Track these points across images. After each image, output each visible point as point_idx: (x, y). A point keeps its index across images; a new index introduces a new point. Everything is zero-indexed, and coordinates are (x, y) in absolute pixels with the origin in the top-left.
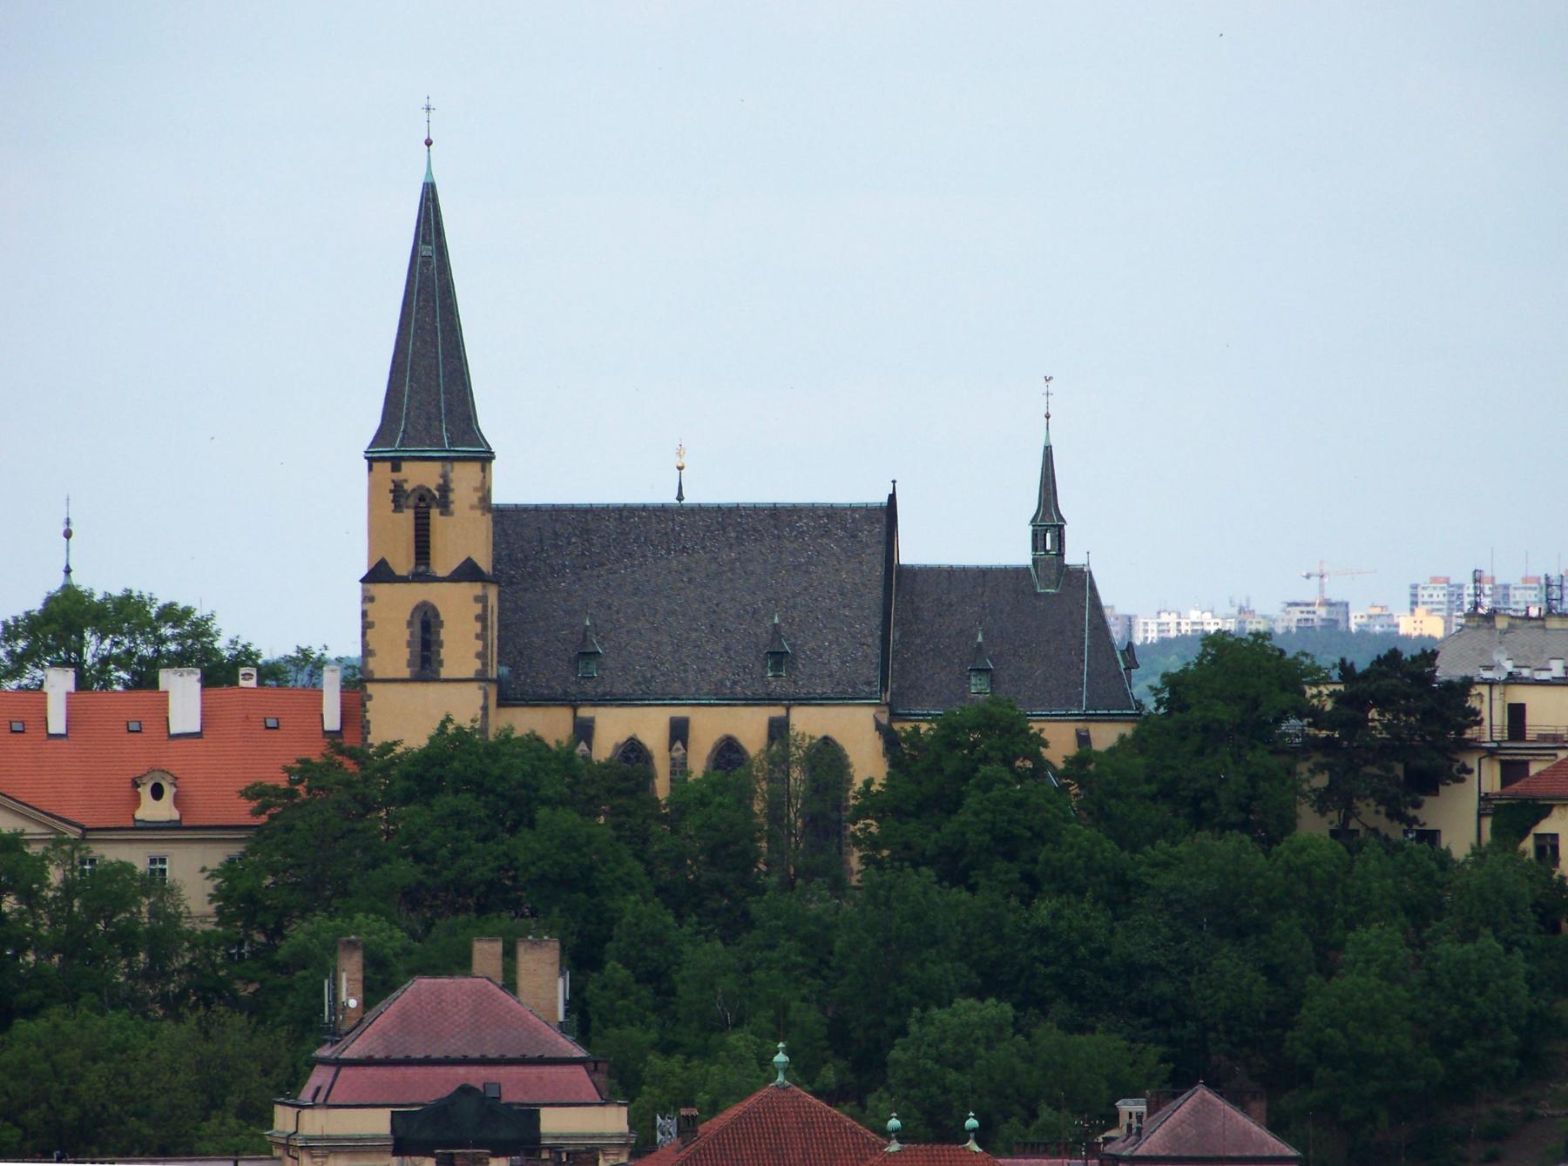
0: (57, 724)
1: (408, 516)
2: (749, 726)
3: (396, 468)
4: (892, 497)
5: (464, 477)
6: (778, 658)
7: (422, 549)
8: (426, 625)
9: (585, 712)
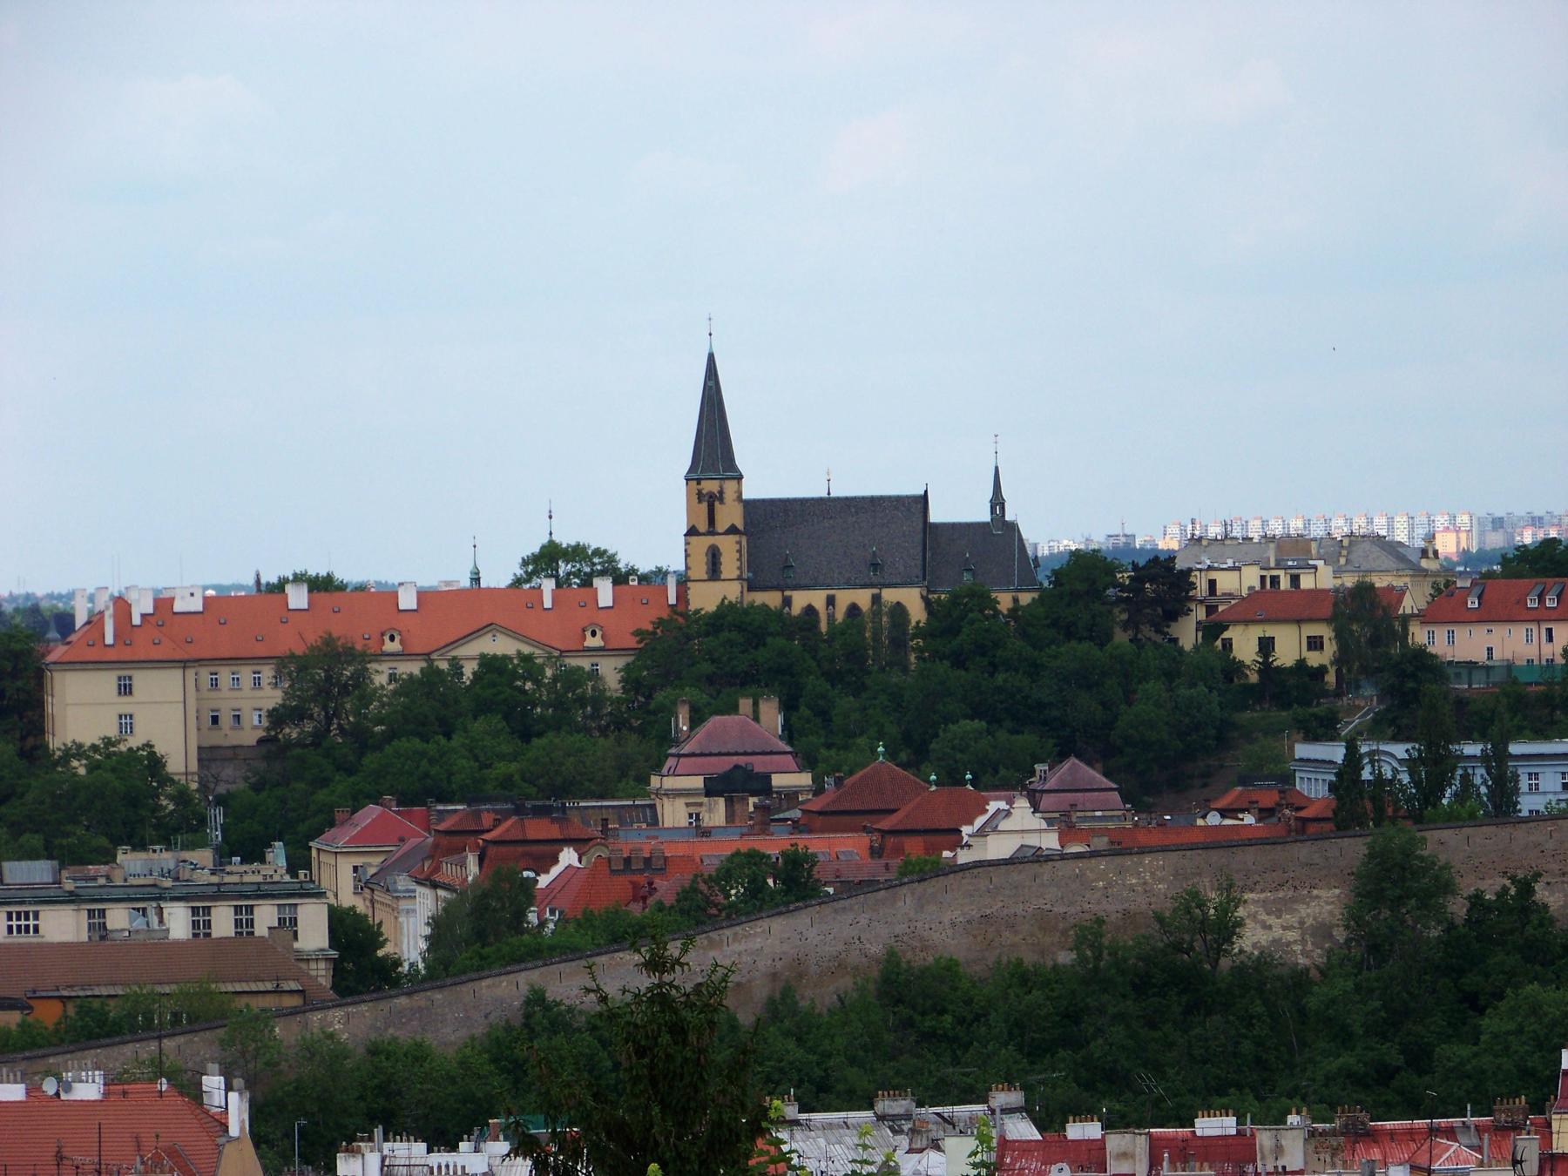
1: (705, 505)
5: (730, 487)
8: (714, 556)
9: (787, 593)
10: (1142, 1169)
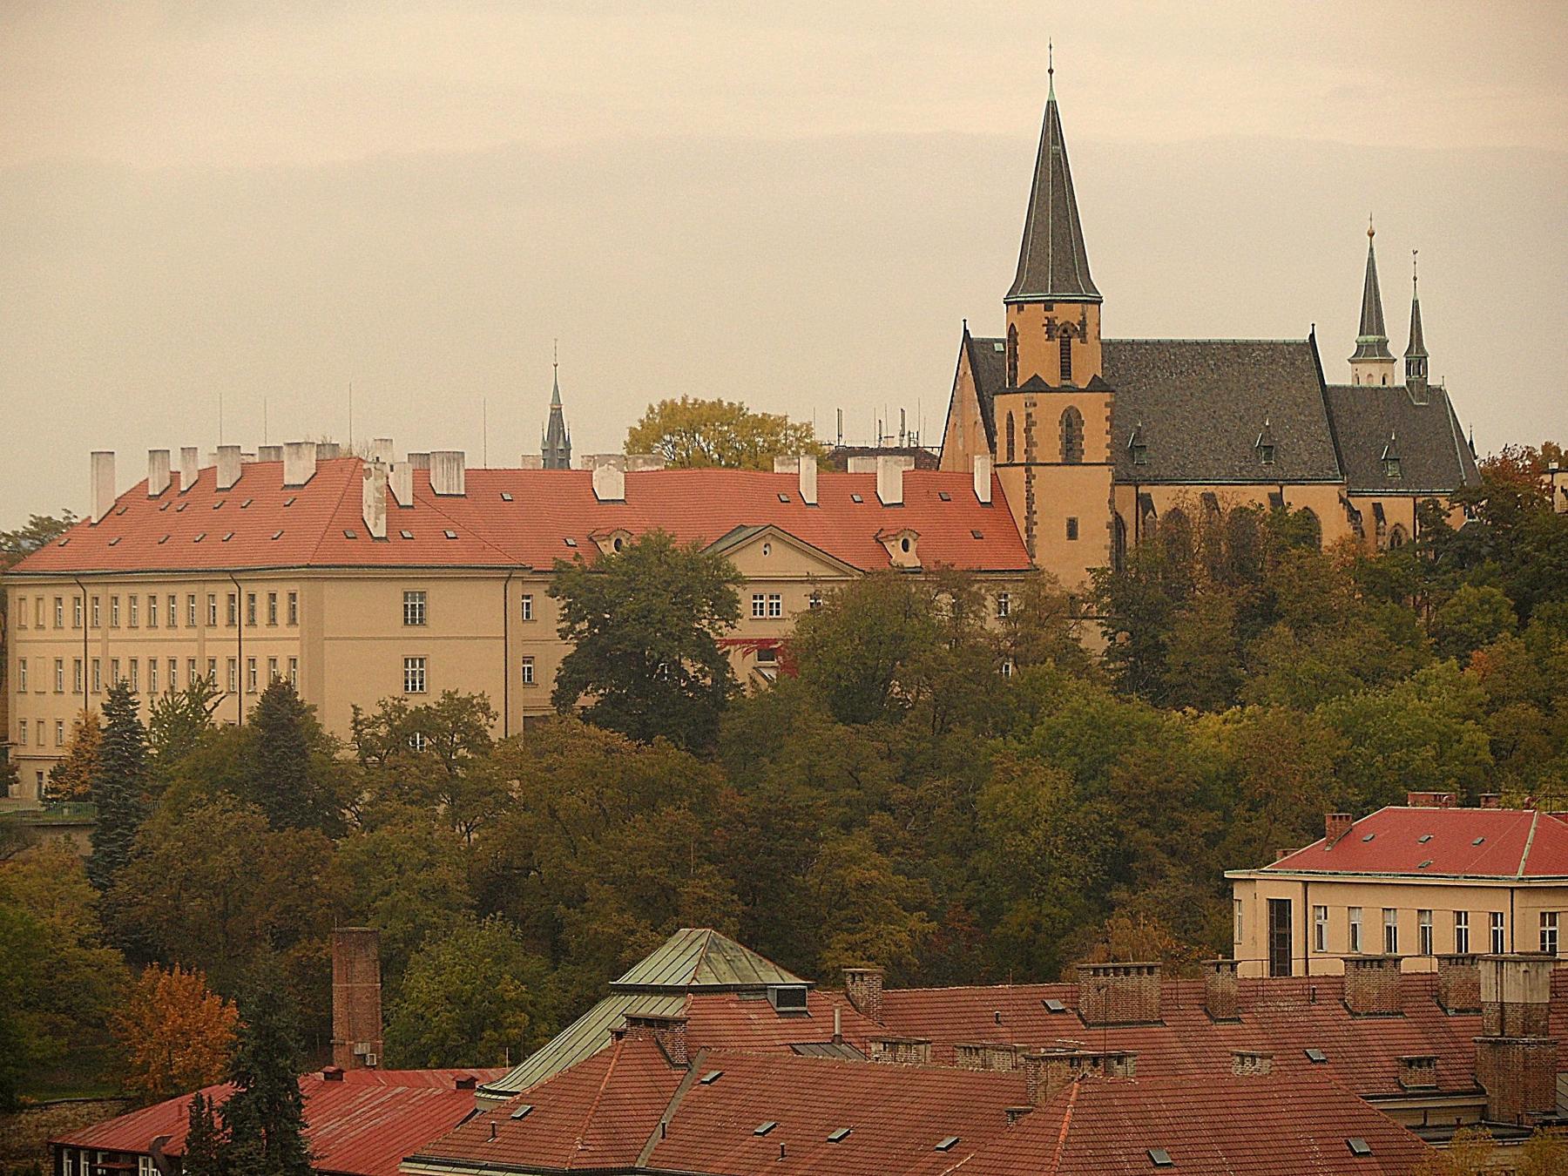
0: (811, 498)
2: (1257, 495)
3: (1048, 308)
4: (1312, 336)
7: (1066, 371)
10: (47, 1168)
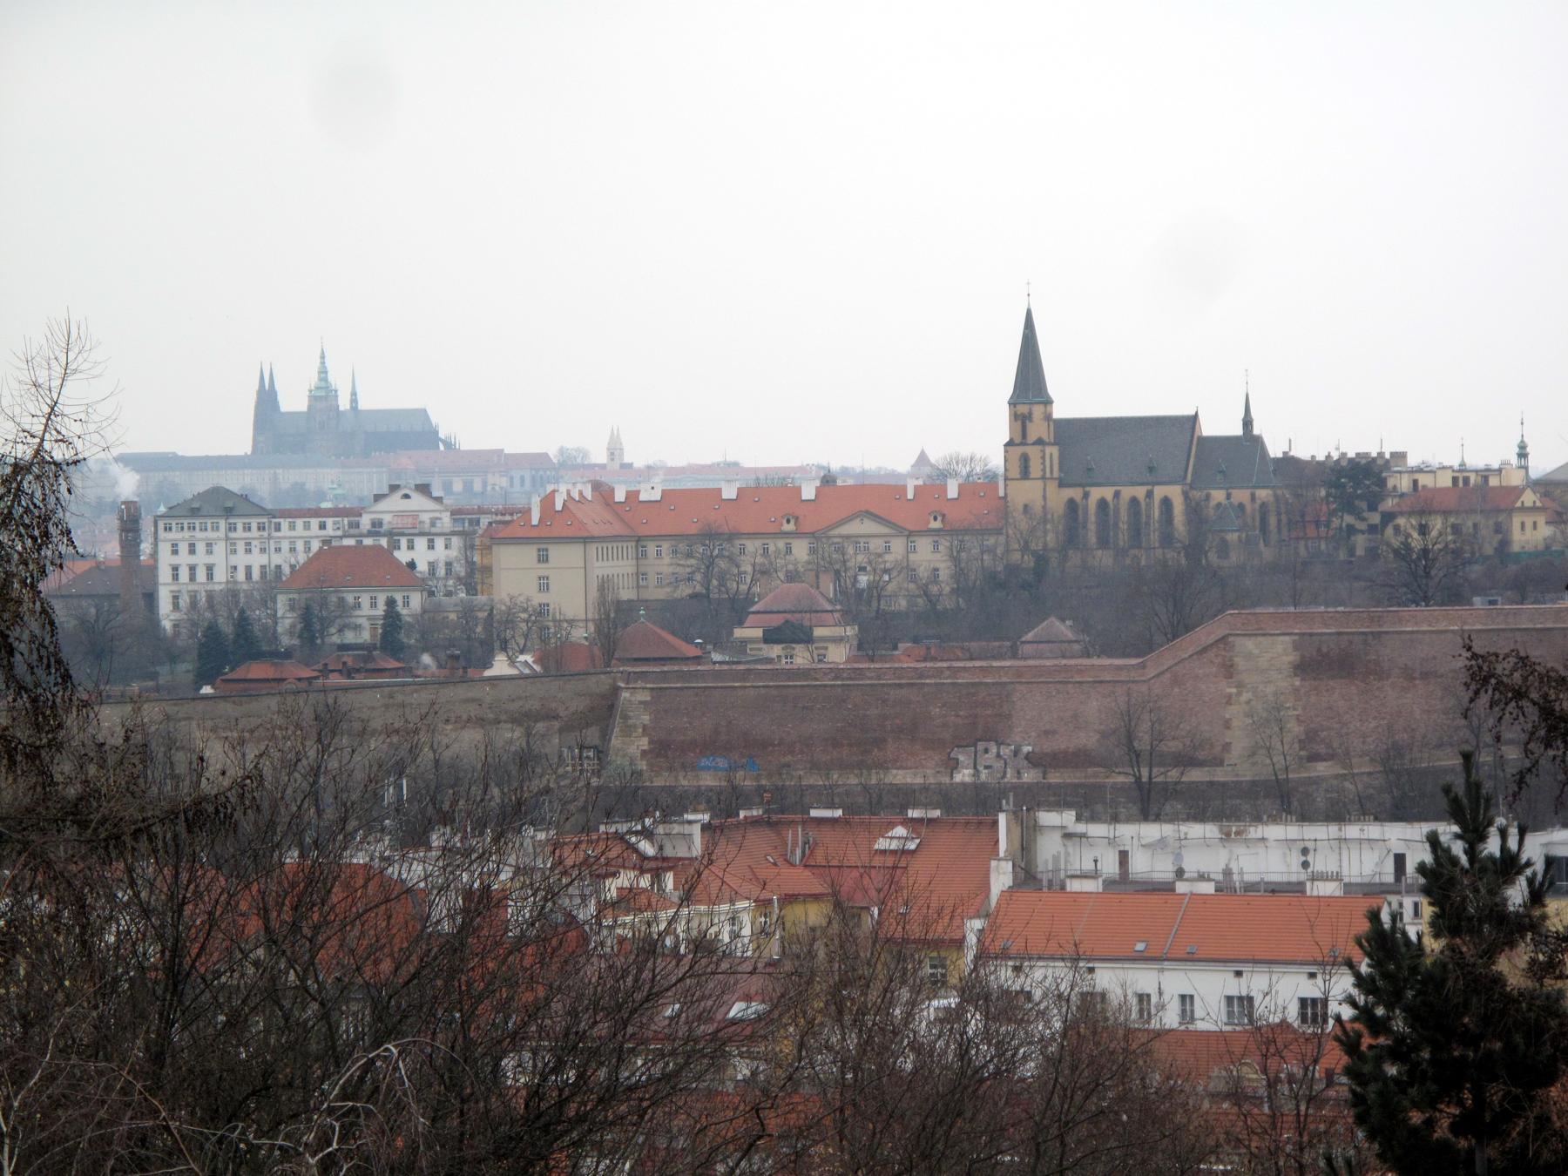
5: (1038, 411)
6: (1151, 469)
7: (1024, 435)
8: (1025, 459)
